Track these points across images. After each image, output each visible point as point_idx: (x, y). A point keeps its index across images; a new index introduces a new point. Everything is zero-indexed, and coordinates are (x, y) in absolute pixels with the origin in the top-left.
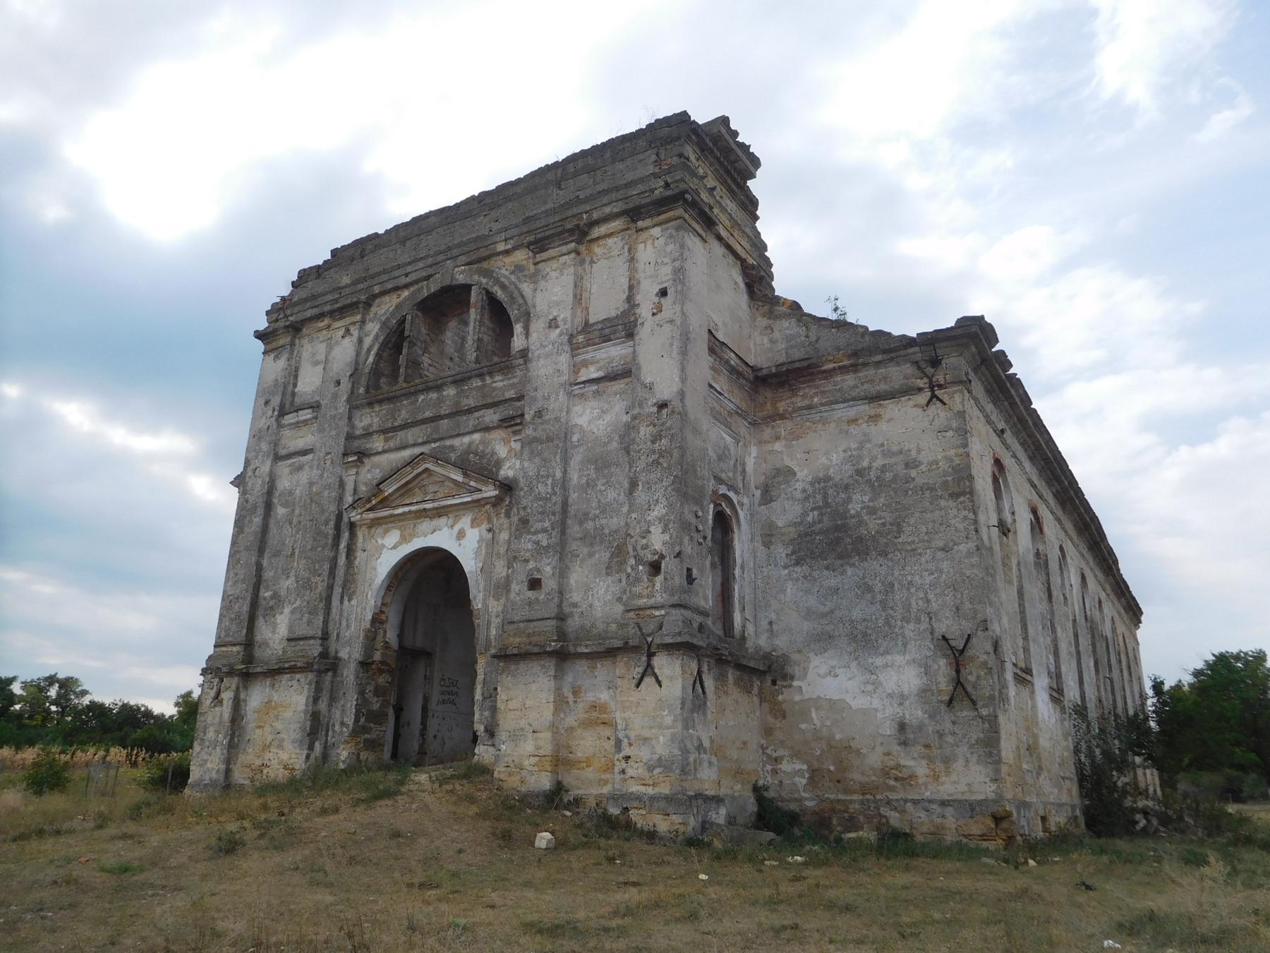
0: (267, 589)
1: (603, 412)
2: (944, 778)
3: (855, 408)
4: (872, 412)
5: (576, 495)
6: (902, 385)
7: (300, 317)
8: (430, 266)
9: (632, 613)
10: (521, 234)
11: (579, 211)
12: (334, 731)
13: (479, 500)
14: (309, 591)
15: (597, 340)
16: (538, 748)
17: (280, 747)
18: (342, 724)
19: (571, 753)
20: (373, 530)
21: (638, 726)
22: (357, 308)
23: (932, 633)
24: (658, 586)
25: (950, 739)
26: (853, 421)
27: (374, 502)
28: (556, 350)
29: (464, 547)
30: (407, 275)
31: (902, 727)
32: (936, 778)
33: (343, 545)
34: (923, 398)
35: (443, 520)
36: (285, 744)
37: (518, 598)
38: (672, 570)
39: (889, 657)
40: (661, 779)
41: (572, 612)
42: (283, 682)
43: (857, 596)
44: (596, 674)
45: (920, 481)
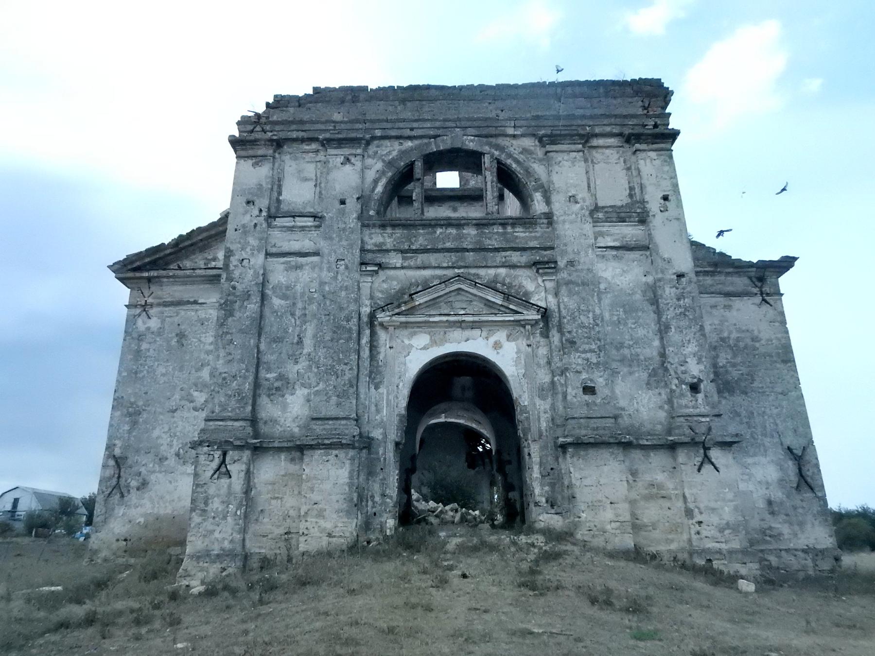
0: (269, 370)
1: (624, 271)
3: (713, 299)
4: (726, 303)
7: (282, 135)
8: (438, 128)
9: (682, 418)
11: (583, 123)
12: (374, 503)
14: (333, 378)
16: (617, 515)
17: (321, 514)
19: (637, 519)
20: (397, 331)
24: (700, 401)
25: (800, 510)
26: (714, 307)
27: (403, 308)
29: (503, 355)
30: (412, 129)
31: (770, 503)
32: (796, 535)
33: (365, 340)
34: (758, 299)
35: (477, 332)
36: (326, 514)
37: (575, 400)
42: (316, 457)
43: (731, 418)
45: (762, 350)
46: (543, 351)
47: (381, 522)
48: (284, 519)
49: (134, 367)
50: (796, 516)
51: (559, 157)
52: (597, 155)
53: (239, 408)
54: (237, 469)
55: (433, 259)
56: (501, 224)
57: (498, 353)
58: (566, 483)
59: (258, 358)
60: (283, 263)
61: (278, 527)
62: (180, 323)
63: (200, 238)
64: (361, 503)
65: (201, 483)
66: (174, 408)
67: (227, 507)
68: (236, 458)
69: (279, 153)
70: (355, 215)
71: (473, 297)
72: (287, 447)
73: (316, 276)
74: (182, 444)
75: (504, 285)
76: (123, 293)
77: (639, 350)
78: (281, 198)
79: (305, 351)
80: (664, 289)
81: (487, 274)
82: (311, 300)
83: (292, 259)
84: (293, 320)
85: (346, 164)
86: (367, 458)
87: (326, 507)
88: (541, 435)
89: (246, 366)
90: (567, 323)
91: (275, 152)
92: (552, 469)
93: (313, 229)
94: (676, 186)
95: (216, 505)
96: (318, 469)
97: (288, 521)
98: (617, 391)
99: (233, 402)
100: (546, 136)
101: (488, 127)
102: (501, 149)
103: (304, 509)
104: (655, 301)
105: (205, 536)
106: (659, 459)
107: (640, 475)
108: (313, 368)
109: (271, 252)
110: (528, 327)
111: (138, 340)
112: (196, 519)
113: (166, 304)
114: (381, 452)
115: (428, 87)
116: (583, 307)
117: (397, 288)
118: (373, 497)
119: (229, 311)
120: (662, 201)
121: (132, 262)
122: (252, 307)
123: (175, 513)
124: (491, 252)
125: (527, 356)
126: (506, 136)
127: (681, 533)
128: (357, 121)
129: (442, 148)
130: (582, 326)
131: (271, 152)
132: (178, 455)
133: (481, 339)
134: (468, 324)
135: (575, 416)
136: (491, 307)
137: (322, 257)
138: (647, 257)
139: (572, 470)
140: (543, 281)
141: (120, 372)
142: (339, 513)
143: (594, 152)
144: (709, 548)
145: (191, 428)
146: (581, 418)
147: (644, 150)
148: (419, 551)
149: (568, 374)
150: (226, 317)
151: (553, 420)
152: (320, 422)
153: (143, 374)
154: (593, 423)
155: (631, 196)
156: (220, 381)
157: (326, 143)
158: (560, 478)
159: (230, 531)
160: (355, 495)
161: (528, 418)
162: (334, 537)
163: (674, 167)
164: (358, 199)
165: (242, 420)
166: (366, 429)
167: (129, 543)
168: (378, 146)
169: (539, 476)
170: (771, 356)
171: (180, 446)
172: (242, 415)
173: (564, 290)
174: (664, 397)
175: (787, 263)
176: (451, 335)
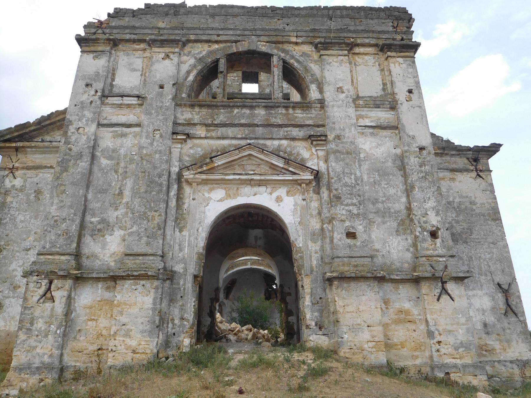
0: (93, 215)
2: (508, 350)
3: (443, 173)
4: (451, 177)
5: (368, 187)
6: (463, 167)
7: (118, 37)
8: (239, 36)
10: (309, 37)
11: (349, 36)
12: (174, 324)
13: (296, 180)
14: (145, 222)
15: (372, 106)
17: (127, 334)
18: (182, 319)
19: (388, 339)
20: (200, 187)
21: (443, 323)
22: (177, 44)
23: (493, 281)
24: (438, 244)
27: (205, 168)
28: (345, 104)
29: (283, 207)
30: (218, 35)
31: (485, 325)
32: (505, 350)
35: (263, 189)
38: (446, 237)
39: (475, 291)
41: (376, 255)
42: (126, 286)
44: (399, 292)
45: (477, 211)
46: (315, 204)
48: (98, 338)
51: (330, 59)
53: (66, 245)
54: (59, 295)
55: (230, 132)
56: (284, 107)
57: (279, 205)
58: (332, 310)
59: (85, 206)
60: (112, 132)
62: (38, 182)
63: (58, 119)
64: (163, 325)
65: (29, 306)
66: (29, 247)
67: (49, 326)
69: (115, 50)
70: (170, 97)
71: (260, 161)
72: (103, 278)
75: (285, 153)
77: (390, 205)
78: (114, 83)
79: (124, 201)
84: (116, 176)
85: (166, 59)
86: (169, 288)
87: (133, 328)
88: (312, 271)
89: (75, 211)
90: (335, 183)
91: (112, 49)
92: (320, 298)
94: (418, 84)
95: (40, 325)
96: (128, 296)
97: (101, 339)
98: (373, 237)
100: (320, 43)
101: (276, 35)
103: (114, 329)
104: (402, 168)
107: (391, 304)
109: (103, 123)
110: (304, 185)
111: (5, 194)
113: (28, 168)
115: (232, 7)
116: (346, 170)
117: (201, 153)
118: (173, 320)
120: (408, 94)
122: (84, 164)
125: (302, 208)
128: (176, 28)
129: (241, 50)
130: (346, 185)
131: (108, 48)
133: (266, 194)
134: (256, 182)
136: (274, 169)
139: (336, 299)
140: (316, 150)
142: (143, 333)
143: (356, 58)
144: (447, 364)
146: (344, 257)
147: (394, 57)
149: (334, 222)
151: (322, 258)
152: (132, 258)
155: (384, 90)
156: (52, 222)
157: (152, 43)
158: (327, 305)
159: (50, 347)
161: (302, 257)
162: (138, 353)
164: (174, 84)
165: (67, 254)
166: (169, 264)
168: (192, 48)
169: (310, 304)
170: (484, 216)
172: (68, 251)
173: (332, 157)
174: (410, 241)
175: (494, 149)
176: (242, 190)
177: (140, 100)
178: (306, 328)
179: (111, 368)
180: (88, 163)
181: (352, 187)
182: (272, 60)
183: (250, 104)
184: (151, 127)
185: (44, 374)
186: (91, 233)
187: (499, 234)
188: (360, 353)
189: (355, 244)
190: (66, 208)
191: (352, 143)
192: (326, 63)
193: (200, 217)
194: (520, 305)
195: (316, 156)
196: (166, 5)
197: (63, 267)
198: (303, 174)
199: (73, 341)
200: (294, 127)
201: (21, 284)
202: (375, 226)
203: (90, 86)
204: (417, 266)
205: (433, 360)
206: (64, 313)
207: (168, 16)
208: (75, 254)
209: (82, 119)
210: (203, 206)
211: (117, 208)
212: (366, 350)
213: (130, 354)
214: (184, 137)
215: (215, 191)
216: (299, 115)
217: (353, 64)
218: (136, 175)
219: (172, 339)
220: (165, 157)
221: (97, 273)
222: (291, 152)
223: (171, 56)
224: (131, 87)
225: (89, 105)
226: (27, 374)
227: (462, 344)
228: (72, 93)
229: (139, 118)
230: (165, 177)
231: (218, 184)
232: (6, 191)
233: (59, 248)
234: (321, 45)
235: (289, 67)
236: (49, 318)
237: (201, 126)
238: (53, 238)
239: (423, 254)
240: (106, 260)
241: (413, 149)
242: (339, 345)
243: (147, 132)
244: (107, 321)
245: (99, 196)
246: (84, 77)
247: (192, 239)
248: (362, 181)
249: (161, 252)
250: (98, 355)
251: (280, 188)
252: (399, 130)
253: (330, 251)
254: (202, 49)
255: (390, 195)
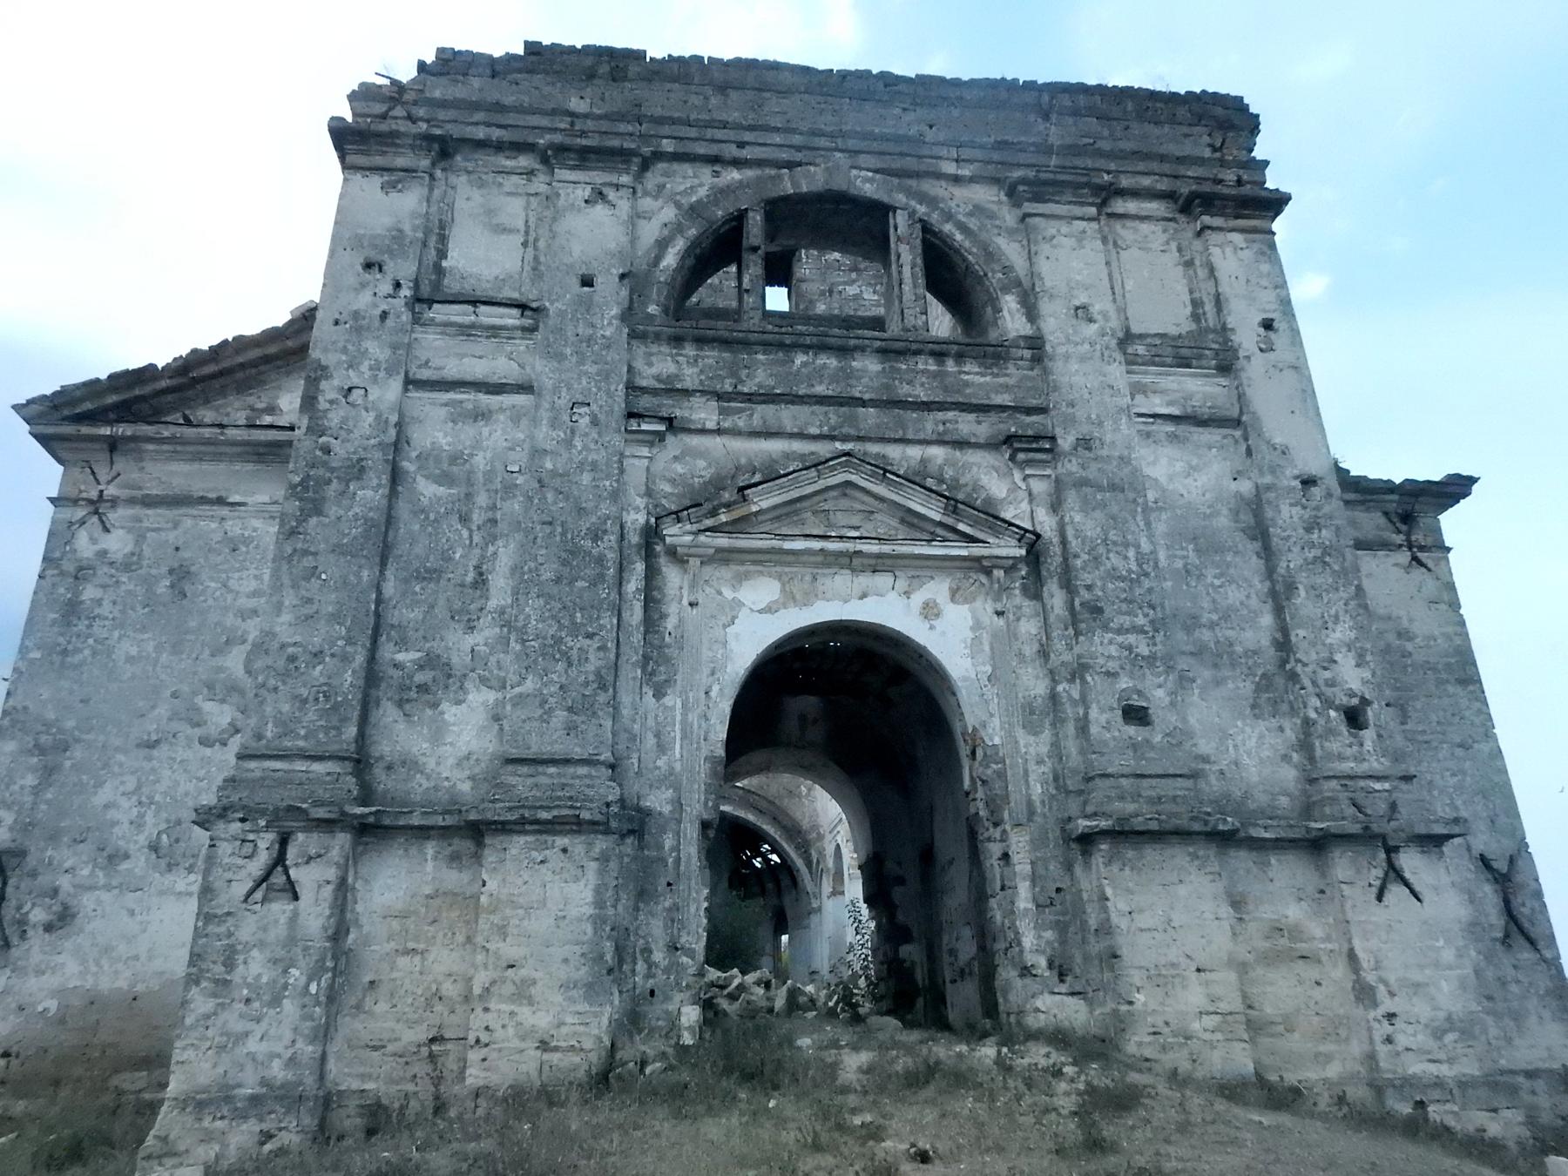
0: (403, 643)
5: (1169, 584)
7: (456, 131)
8: (799, 149)
11: (1097, 165)
12: (651, 965)
13: (978, 559)
14: (560, 666)
17: (523, 994)
18: (674, 948)
20: (708, 570)
24: (1368, 745)
25: (1514, 988)
27: (723, 518)
28: (1098, 354)
29: (943, 633)
30: (741, 145)
32: (1509, 1040)
33: (634, 584)
35: (884, 580)
40: (1459, 1051)
41: (1203, 770)
42: (514, 851)
44: (1271, 875)
45: (1419, 657)
46: (1029, 627)
47: (667, 1012)
48: (429, 1005)
49: (61, 640)
50: (1506, 1000)
51: (1051, 228)
52: (1124, 231)
53: (326, 729)
54: (312, 878)
55: (788, 416)
56: (933, 354)
57: (932, 628)
58: (1093, 922)
59: (378, 615)
60: (446, 405)
61: (411, 1024)
62: (180, 544)
63: (240, 359)
64: (620, 967)
65: (219, 912)
66: (154, 737)
67: (285, 971)
68: (313, 852)
69: (443, 170)
70: (615, 311)
71: (876, 503)
72: (443, 828)
73: (521, 436)
74: (168, 821)
75: (941, 481)
76: (48, 473)
77: (1230, 633)
78: (444, 264)
79: (493, 603)
80: (1277, 506)
81: (905, 456)
82: (509, 489)
83: (467, 397)
84: (465, 533)
85: (596, 202)
86: (635, 858)
87: (537, 975)
88: (1031, 812)
89: (349, 630)
90: (1083, 569)
91: (433, 164)
92: (1058, 890)
93: (519, 333)
94: (1286, 303)
95: (255, 968)
96: (520, 882)
97: (439, 1008)
98: (1192, 721)
99: (311, 716)
100: (1023, 181)
101: (902, 154)
102: (932, 202)
103: (480, 981)
104: (1260, 533)
105: (222, 1048)
106: (1287, 872)
107: (1251, 907)
108: (512, 644)
109: (418, 376)
110: (999, 573)
111: (76, 578)
112: (201, 1003)
113: (149, 502)
114: (668, 842)
115: (775, 66)
116: (1112, 535)
117: (707, 474)
118: (647, 951)
119: (314, 501)
120: (1262, 330)
121: (74, 402)
122: (370, 494)
123: (140, 988)
124: (914, 410)
125: (995, 636)
126: (939, 176)
127: (1347, 1040)
128: (620, 117)
129: (805, 189)
130: (1113, 575)
131: (425, 163)
132: (154, 848)
133: (892, 595)
134: (866, 561)
135: (1110, 770)
136: (911, 525)
137: (540, 395)
138: (1236, 442)
139: (1109, 892)
140: (1025, 479)
141: (23, 650)
143: (1118, 226)
144: (1414, 1076)
145: (190, 787)
146: (1123, 776)
147: (1220, 229)
148: (776, 1087)
149: (1089, 679)
150: (304, 517)
151: (1056, 779)
152: (525, 770)
153: (81, 656)
154: (1148, 788)
155: (1196, 317)
156: (281, 663)
157: (553, 156)
158: (1078, 910)
159: (288, 1035)
160: (609, 947)
161: (1001, 775)
162: (556, 1049)
163: (1281, 266)
164: (623, 276)
165: (330, 758)
166: (634, 787)
167: (14, 1062)
168: (666, 174)
169: (1030, 906)
170: (1434, 669)
171: (163, 826)
172: (334, 748)
173: (1072, 498)
174: (1290, 734)
175: (1456, 488)
176: (828, 581)
177: (528, 317)
178: (1022, 976)
179: (477, 1096)
180: (385, 491)
181: (1131, 580)
182: (891, 221)
183: (840, 342)
184: (563, 394)
185: (273, 1116)
186: (397, 697)
187: (1477, 721)
188: (1181, 1045)
189: (1148, 741)
190: (323, 622)
191: (1124, 460)
192: (1040, 237)
193: (710, 654)
194: (1540, 917)
195: (1025, 494)
196: (588, 50)
197: (321, 793)
198: (997, 541)
199: (354, 1016)
200: (963, 411)
201: (132, 846)
202: (1196, 691)
203: (377, 269)
204: (1314, 803)
205: (1377, 1065)
206: (330, 932)
207: (595, 82)
208: (355, 756)
209: (359, 364)
210: (721, 623)
211: (472, 624)
212: (1199, 1039)
213: (532, 1053)
214: (663, 428)
215: (752, 582)
216: (974, 377)
217: (1111, 243)
218: (528, 531)
219: (645, 1008)
220: (608, 483)
221: (426, 813)
222: (957, 481)
223: (612, 195)
224: (496, 278)
225: (377, 323)
226: (222, 1118)
227: (1450, 1023)
228: (324, 285)
229: (523, 368)
230: (611, 539)
231: (759, 563)
232: (81, 569)
233: (306, 738)
234: (1026, 188)
235: (937, 242)
236: (284, 947)
237: (704, 399)
238: (286, 708)
239: (1331, 770)
240: (444, 775)
241: (1286, 483)
242: (1123, 1021)
243: (553, 407)
244: (454, 954)
245: (417, 589)
246: (357, 242)
247: (693, 717)
248: (1156, 565)
249: (609, 754)
250: (432, 1057)
251: (932, 578)
252: (1245, 430)
253: (1080, 759)
254: (696, 181)
255: (1229, 608)
